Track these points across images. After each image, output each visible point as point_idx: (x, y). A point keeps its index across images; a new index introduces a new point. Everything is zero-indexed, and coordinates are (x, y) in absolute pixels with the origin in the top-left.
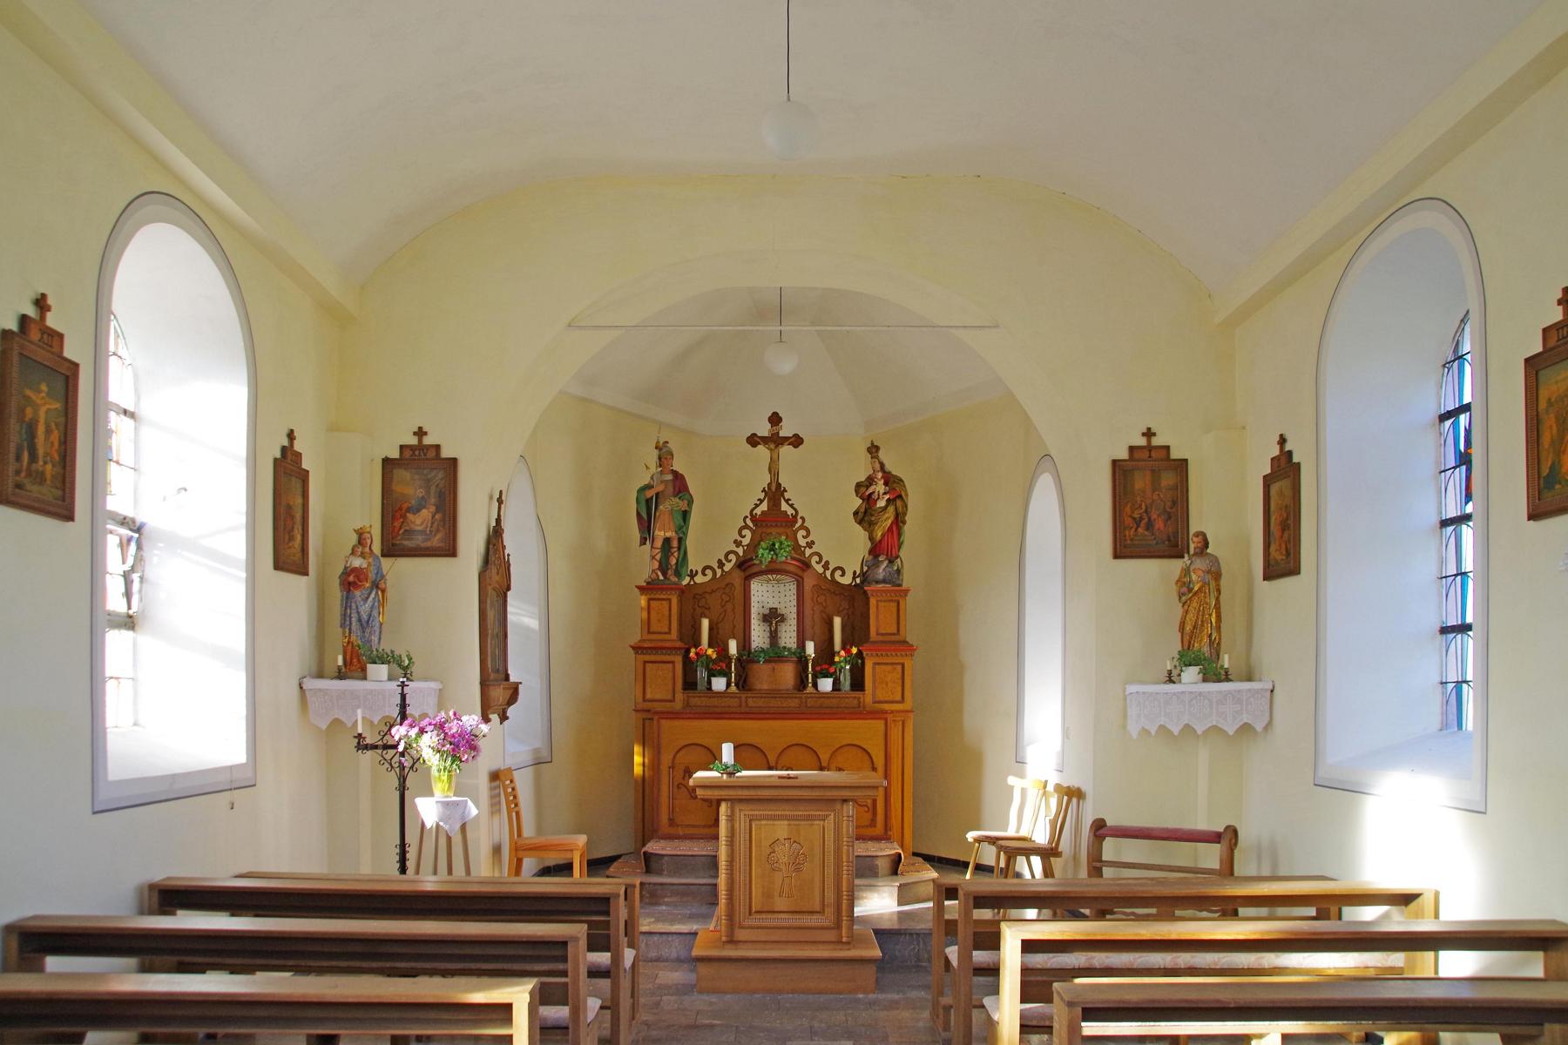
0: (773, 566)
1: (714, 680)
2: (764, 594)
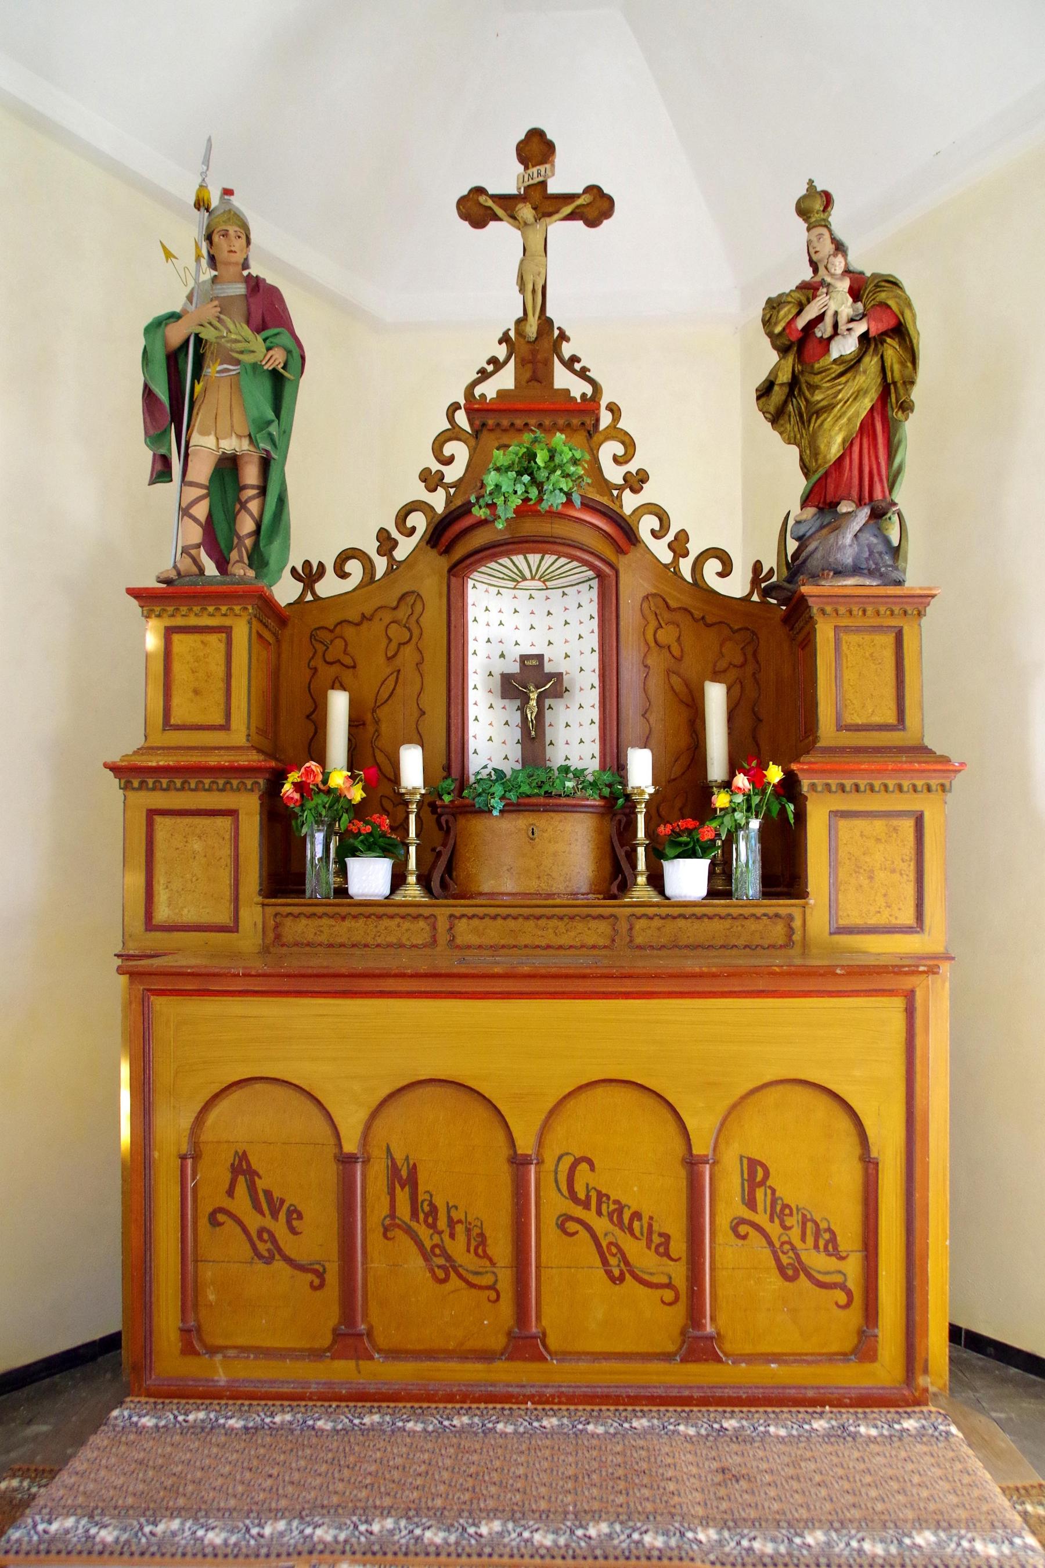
0: (530, 527)
1: (354, 865)
2: (509, 617)
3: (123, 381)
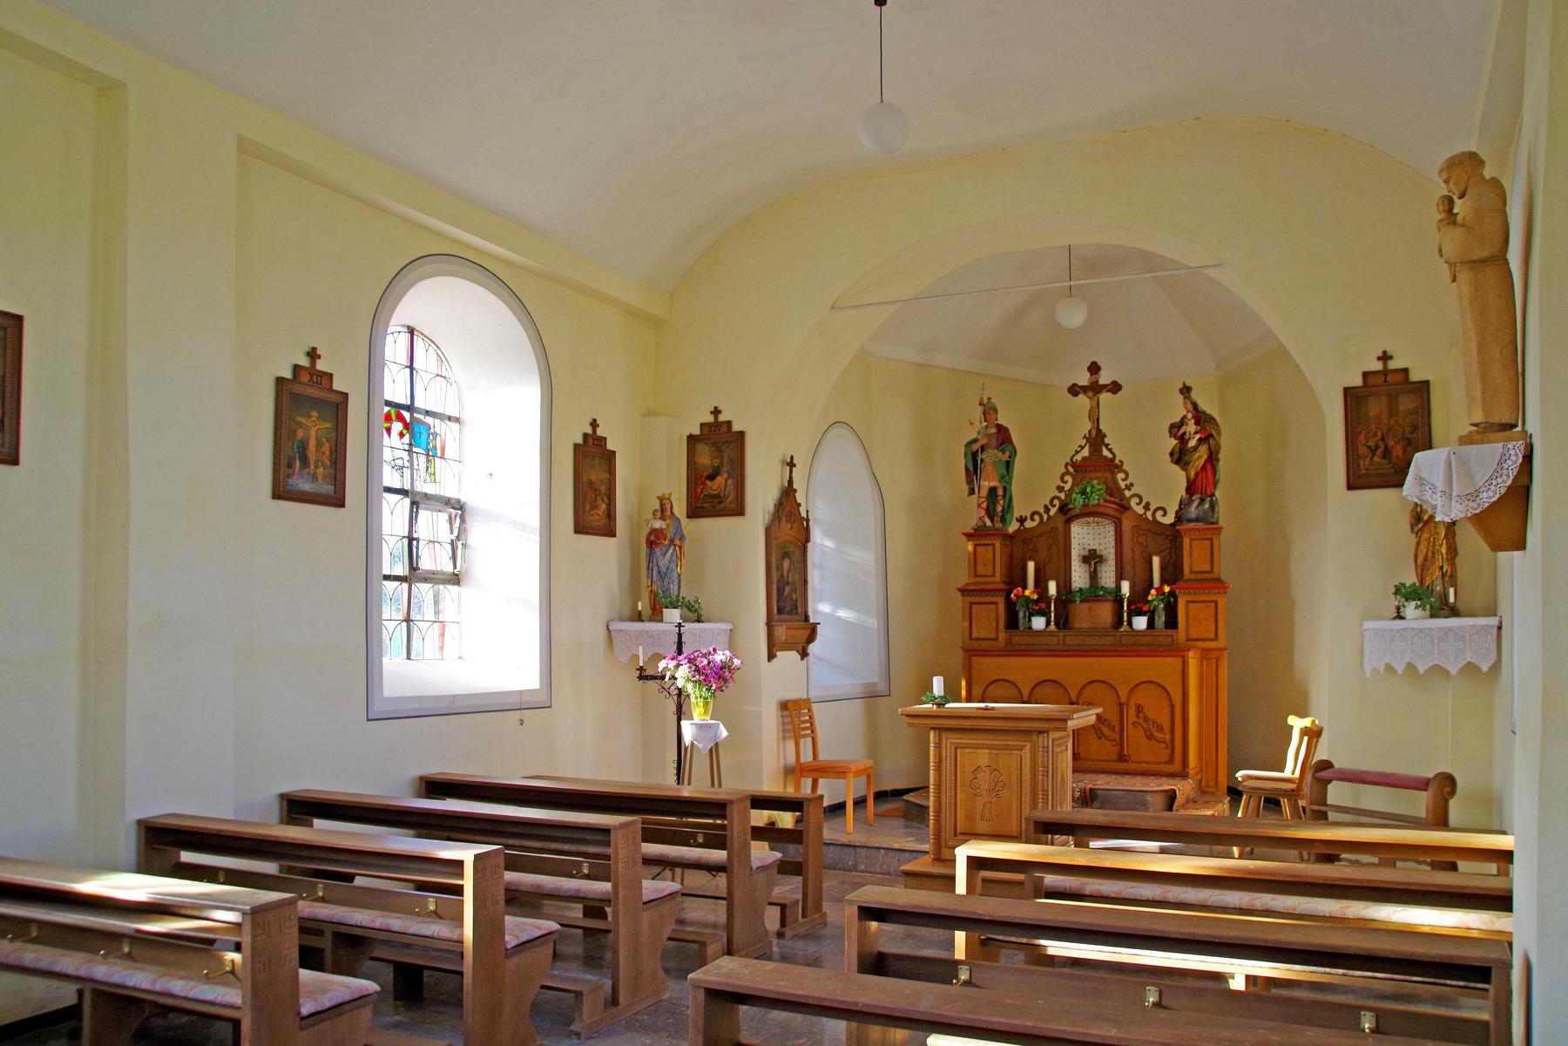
1: (1034, 619)
2: (1082, 536)
3: (960, 463)
